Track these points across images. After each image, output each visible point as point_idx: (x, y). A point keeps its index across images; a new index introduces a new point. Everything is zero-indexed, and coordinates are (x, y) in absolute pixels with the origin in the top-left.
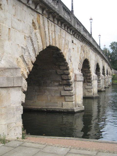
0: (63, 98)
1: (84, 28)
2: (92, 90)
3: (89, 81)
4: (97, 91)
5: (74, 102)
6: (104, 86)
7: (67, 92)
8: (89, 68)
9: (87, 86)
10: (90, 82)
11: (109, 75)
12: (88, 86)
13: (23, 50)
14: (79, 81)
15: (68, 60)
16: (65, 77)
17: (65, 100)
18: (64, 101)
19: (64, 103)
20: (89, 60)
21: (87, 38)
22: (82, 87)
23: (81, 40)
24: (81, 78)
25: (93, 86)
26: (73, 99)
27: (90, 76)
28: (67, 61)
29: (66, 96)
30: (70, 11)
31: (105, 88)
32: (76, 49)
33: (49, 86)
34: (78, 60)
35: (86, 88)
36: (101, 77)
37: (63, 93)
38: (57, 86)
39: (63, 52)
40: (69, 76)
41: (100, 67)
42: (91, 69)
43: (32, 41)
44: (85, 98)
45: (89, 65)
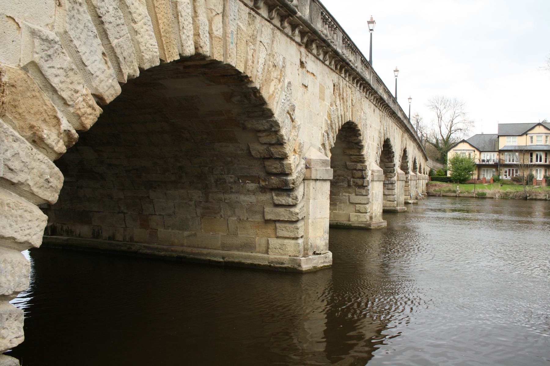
0: (271, 227)
1: (346, 39)
2: (367, 206)
3: (359, 182)
4: (382, 211)
5: (300, 241)
6: (402, 199)
7: (281, 210)
8: (359, 146)
9: (356, 197)
10: (363, 186)
11: (420, 172)
12: (359, 197)
13: (37, 42)
14: (320, 180)
15: (279, 115)
16: (275, 166)
17: (276, 234)
18: (273, 235)
19: (273, 242)
20: (360, 127)
21: (356, 67)
22: (328, 196)
23: (333, 67)
24: (324, 170)
25: (369, 196)
26: (299, 232)
27: (364, 169)
28: (275, 115)
29: (279, 221)
30: (367, 61)
31: (406, 203)
32: (314, 88)
33: (232, 192)
34: (322, 121)
35: (352, 201)
36: (396, 176)
37: (271, 213)
38: (254, 193)
39: (258, 87)
40: (285, 162)
41: (394, 150)
42: (364, 152)
43: (99, 20)
44: (334, 228)
45: (360, 141)
